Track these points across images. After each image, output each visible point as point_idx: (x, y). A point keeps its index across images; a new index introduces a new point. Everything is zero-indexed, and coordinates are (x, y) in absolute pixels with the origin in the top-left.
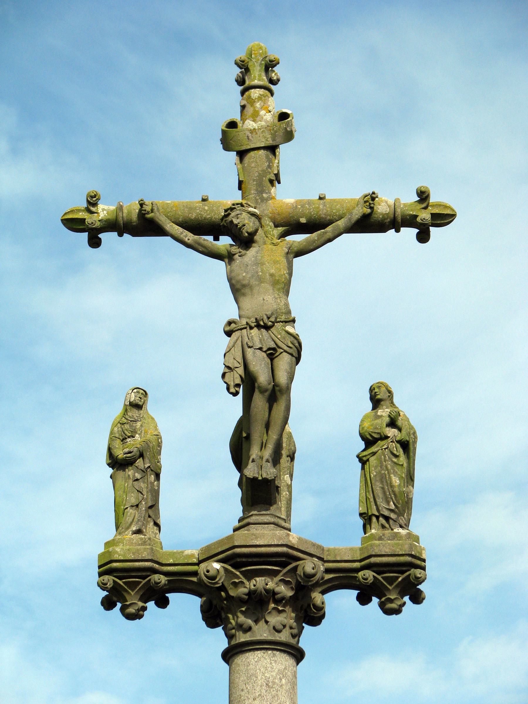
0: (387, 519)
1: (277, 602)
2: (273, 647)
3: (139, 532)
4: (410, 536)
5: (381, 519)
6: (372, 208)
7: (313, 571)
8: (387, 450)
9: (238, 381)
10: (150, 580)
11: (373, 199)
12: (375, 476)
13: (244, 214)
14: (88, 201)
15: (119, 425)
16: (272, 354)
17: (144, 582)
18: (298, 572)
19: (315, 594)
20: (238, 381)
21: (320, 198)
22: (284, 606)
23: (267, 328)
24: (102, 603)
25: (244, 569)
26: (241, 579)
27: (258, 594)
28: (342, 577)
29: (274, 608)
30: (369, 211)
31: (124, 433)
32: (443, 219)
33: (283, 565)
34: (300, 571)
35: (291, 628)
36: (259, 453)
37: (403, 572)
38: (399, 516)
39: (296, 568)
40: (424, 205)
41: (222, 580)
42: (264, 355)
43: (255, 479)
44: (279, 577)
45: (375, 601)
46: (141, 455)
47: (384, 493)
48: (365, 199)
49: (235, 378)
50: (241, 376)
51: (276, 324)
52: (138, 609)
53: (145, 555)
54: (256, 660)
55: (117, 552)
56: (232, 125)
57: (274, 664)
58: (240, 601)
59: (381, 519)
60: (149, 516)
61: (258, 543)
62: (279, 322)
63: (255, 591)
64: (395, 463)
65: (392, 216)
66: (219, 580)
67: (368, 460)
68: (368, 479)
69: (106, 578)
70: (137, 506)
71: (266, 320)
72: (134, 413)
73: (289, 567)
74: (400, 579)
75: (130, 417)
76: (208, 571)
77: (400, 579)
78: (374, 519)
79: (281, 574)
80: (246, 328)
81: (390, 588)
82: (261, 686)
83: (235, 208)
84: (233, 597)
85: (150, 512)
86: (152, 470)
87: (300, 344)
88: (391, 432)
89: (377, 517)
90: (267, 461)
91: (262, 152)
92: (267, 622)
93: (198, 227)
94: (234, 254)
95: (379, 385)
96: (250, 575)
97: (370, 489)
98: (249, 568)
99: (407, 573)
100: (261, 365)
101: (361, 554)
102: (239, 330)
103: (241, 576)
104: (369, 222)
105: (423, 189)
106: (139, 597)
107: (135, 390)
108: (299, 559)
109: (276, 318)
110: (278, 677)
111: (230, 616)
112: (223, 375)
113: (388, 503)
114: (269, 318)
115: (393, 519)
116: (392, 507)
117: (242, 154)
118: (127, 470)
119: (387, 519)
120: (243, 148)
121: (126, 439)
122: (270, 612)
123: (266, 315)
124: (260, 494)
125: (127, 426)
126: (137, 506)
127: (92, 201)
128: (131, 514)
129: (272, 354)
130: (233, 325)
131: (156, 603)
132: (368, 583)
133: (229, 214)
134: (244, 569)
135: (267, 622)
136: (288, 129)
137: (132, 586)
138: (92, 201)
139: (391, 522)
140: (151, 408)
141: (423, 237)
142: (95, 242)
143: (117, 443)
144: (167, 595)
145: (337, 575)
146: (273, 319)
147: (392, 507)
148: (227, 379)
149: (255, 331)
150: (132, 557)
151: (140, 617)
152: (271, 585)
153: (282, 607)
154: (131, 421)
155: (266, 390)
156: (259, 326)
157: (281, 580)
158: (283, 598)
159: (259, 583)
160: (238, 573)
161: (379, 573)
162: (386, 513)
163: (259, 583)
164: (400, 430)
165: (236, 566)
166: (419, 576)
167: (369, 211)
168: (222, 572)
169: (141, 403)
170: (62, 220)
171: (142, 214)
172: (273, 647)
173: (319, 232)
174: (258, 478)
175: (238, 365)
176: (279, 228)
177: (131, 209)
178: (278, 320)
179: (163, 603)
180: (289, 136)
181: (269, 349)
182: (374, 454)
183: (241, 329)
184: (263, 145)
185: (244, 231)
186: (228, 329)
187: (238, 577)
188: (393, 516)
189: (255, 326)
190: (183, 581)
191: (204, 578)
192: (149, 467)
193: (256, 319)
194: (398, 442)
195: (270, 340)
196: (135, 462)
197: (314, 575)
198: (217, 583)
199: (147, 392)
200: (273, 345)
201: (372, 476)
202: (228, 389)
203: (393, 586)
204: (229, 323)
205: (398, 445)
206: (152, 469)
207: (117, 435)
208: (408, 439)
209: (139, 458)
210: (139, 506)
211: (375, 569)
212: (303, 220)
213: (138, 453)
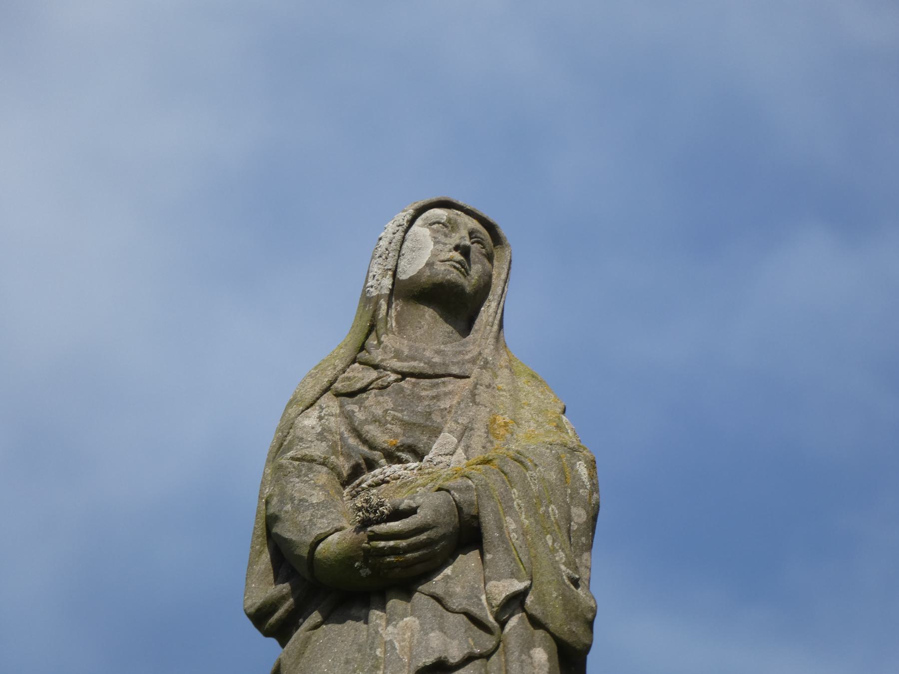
31: (359, 435)
61: (500, 292)
72: (426, 336)
75: (398, 355)
86: (536, 623)
100: (317, 641)
121: (371, 465)
125: (376, 404)
154: (404, 375)
169: (469, 283)
192: (516, 601)
196: (428, 575)
199: (504, 230)
206: (537, 611)
207: (318, 450)
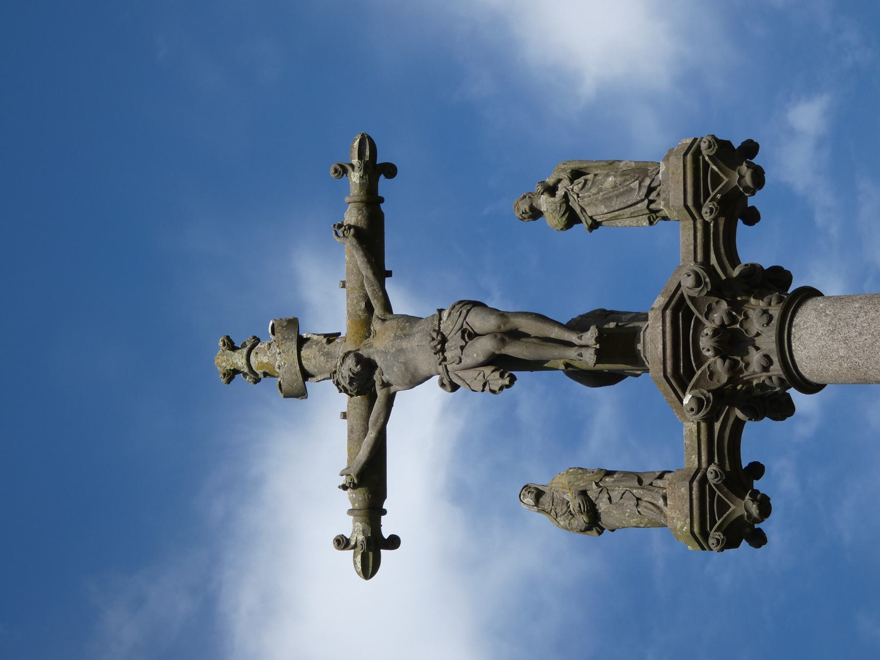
2: (787, 326)
4: (667, 159)
5: (651, 198)
6: (350, 227)
9: (497, 374)
12: (605, 207)
15: (558, 519)
16: (469, 335)
17: (718, 493)
18: (696, 295)
20: (497, 374)
21: (344, 286)
23: (444, 340)
24: (758, 546)
28: (718, 241)
29: (741, 325)
30: (352, 230)
33: (689, 314)
34: (694, 293)
37: (706, 165)
38: (647, 175)
39: (692, 299)
40: (350, 169)
41: (705, 392)
43: (597, 352)
44: (703, 319)
45: (751, 201)
47: (622, 194)
48: (341, 235)
49: (496, 380)
50: (493, 371)
52: (753, 501)
55: (682, 527)
57: (808, 324)
58: (734, 370)
59: (651, 198)
60: (651, 484)
61: (661, 347)
62: (439, 328)
63: (715, 349)
64: (593, 183)
66: (705, 396)
67: (591, 217)
68: (610, 215)
69: (711, 541)
70: (638, 499)
71: (436, 343)
72: (545, 500)
74: (714, 168)
76: (692, 410)
78: (653, 206)
79: (700, 317)
80: (446, 366)
81: (726, 179)
82: (833, 340)
85: (646, 482)
86: (601, 480)
87: (461, 302)
88: (560, 193)
89: (651, 202)
90: (580, 338)
92: (758, 334)
94: (383, 381)
96: (700, 360)
97: (621, 212)
99: (707, 158)
101: (687, 219)
103: (703, 368)
108: (682, 294)
109: (434, 330)
111: (755, 383)
113: (632, 190)
114: (433, 339)
119: (651, 190)
120: (299, 375)
124: (618, 347)
126: (638, 499)
127: (342, 543)
129: (469, 335)
130: (446, 382)
131: (758, 479)
132: (716, 209)
133: (343, 387)
135: (758, 334)
136: (285, 324)
138: (342, 543)
141: (390, 171)
143: (575, 523)
144: (744, 464)
146: (434, 335)
148: (496, 388)
149: (448, 354)
152: (708, 331)
156: (443, 350)
157: (707, 318)
158: (729, 314)
159: (706, 343)
160: (699, 372)
162: (644, 191)
163: (706, 343)
164: (559, 181)
167: (352, 230)
169: (535, 492)
172: (787, 326)
174: (596, 350)
175: (482, 374)
177: (345, 501)
179: (757, 470)
181: (463, 338)
182: (583, 210)
183: (447, 372)
186: (449, 388)
187: (704, 373)
188: (647, 182)
190: (723, 446)
191: (701, 414)
192: (597, 484)
193: (435, 354)
195: (455, 337)
197: (697, 274)
201: (606, 211)
202: (508, 386)
203: (724, 178)
204: (443, 385)
207: (567, 522)
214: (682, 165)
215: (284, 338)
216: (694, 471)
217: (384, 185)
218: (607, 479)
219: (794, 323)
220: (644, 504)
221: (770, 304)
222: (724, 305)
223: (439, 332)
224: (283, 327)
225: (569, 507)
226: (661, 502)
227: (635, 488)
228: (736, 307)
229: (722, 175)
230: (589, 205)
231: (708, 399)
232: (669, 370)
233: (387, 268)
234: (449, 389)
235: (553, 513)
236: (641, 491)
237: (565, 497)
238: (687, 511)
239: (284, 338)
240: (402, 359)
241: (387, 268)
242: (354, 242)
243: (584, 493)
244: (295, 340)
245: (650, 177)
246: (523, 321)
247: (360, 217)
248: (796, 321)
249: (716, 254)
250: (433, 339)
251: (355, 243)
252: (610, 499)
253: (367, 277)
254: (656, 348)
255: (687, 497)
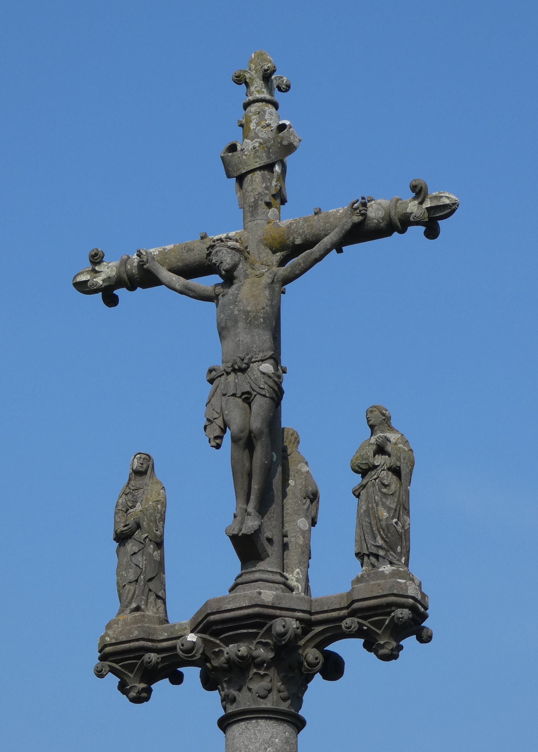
0: (377, 556)
1: (259, 666)
2: (266, 716)
3: (138, 609)
6: (364, 215)
7: (283, 630)
8: (377, 481)
10: (143, 660)
11: (364, 205)
13: (224, 250)
14: (91, 261)
15: (124, 496)
17: (140, 662)
19: (308, 649)
22: (267, 669)
23: (243, 370)
25: (222, 637)
26: (120, 666)
27: (266, 657)
29: (256, 674)
30: (361, 218)
32: (448, 210)
33: (260, 626)
35: (279, 691)
36: (245, 506)
38: (387, 551)
42: (240, 400)
46: (138, 526)
51: (251, 365)
52: (138, 692)
53: (136, 634)
54: (240, 732)
56: (233, 148)
60: (150, 590)
61: (229, 607)
62: (255, 362)
65: (388, 218)
70: (137, 581)
72: (138, 482)
73: (265, 628)
74: (387, 621)
77: (387, 621)
81: (380, 632)
83: (214, 245)
84: (216, 667)
85: (151, 585)
88: (379, 460)
91: (258, 173)
92: (250, 690)
93: (190, 271)
95: (372, 409)
98: (226, 635)
102: (218, 377)
103: (221, 644)
104: (360, 231)
105: (414, 183)
106: (139, 679)
107: (138, 456)
110: (263, 747)
112: (205, 427)
113: (375, 538)
115: (381, 557)
116: (380, 542)
117: (240, 179)
118: (127, 544)
119: (377, 556)
121: (128, 510)
122: (251, 678)
123: (240, 358)
126: (137, 581)
128: (129, 590)
130: (214, 373)
133: (211, 252)
134: (222, 637)
137: (137, 666)
139: (380, 559)
140: (160, 471)
142: (111, 300)
145: (328, 626)
146: (246, 361)
147: (380, 542)
149: (232, 376)
150: (124, 638)
151: (396, 657)
153: (264, 671)
154: (133, 490)
155: (240, 439)
156: (234, 370)
158: (263, 662)
160: (218, 642)
161: (365, 618)
162: (374, 550)
164: (389, 455)
165: (215, 634)
166: (401, 616)
167: (361, 218)
168: (200, 643)
170: (74, 284)
171: (141, 265)
173: (304, 254)
176: (277, 254)
178: (253, 360)
180: (290, 148)
181: (243, 394)
184: (257, 165)
185: (221, 269)
187: (218, 646)
188: (381, 553)
189: (232, 371)
192: (147, 537)
194: (389, 469)
197: (285, 634)
198: (194, 656)
200: (248, 389)
204: (210, 371)
205: (390, 473)
208: (398, 464)
209: (138, 529)
210: (139, 580)
211: (360, 615)
212: (298, 241)
213: (135, 526)
214: (385, 593)
215: (269, 149)
216: (155, 638)
217: (416, 232)
218: (152, 546)
219: (259, 721)
220: (132, 588)
221: (279, 691)
222: (271, 655)
223: (250, 361)
224: (281, 143)
225: (131, 508)
226: (134, 605)
227: (144, 577)
228: (271, 663)
229: (383, 628)
230: (367, 493)
231: (194, 656)
232: (212, 618)
233: (344, 248)
234: (208, 378)
235: (128, 491)
236: (142, 583)
237: (138, 504)
238: (123, 638)
239: (269, 149)
240: (229, 324)
241: (344, 248)
242: (348, 226)
243: (138, 526)
244: (269, 161)
245: (386, 554)
246: (259, 454)
247: (375, 221)
248: (262, 722)
249: (327, 628)
250: (243, 360)
251: (346, 227)
252: (135, 553)
253: (311, 253)
254: (229, 603)
255: (132, 637)
